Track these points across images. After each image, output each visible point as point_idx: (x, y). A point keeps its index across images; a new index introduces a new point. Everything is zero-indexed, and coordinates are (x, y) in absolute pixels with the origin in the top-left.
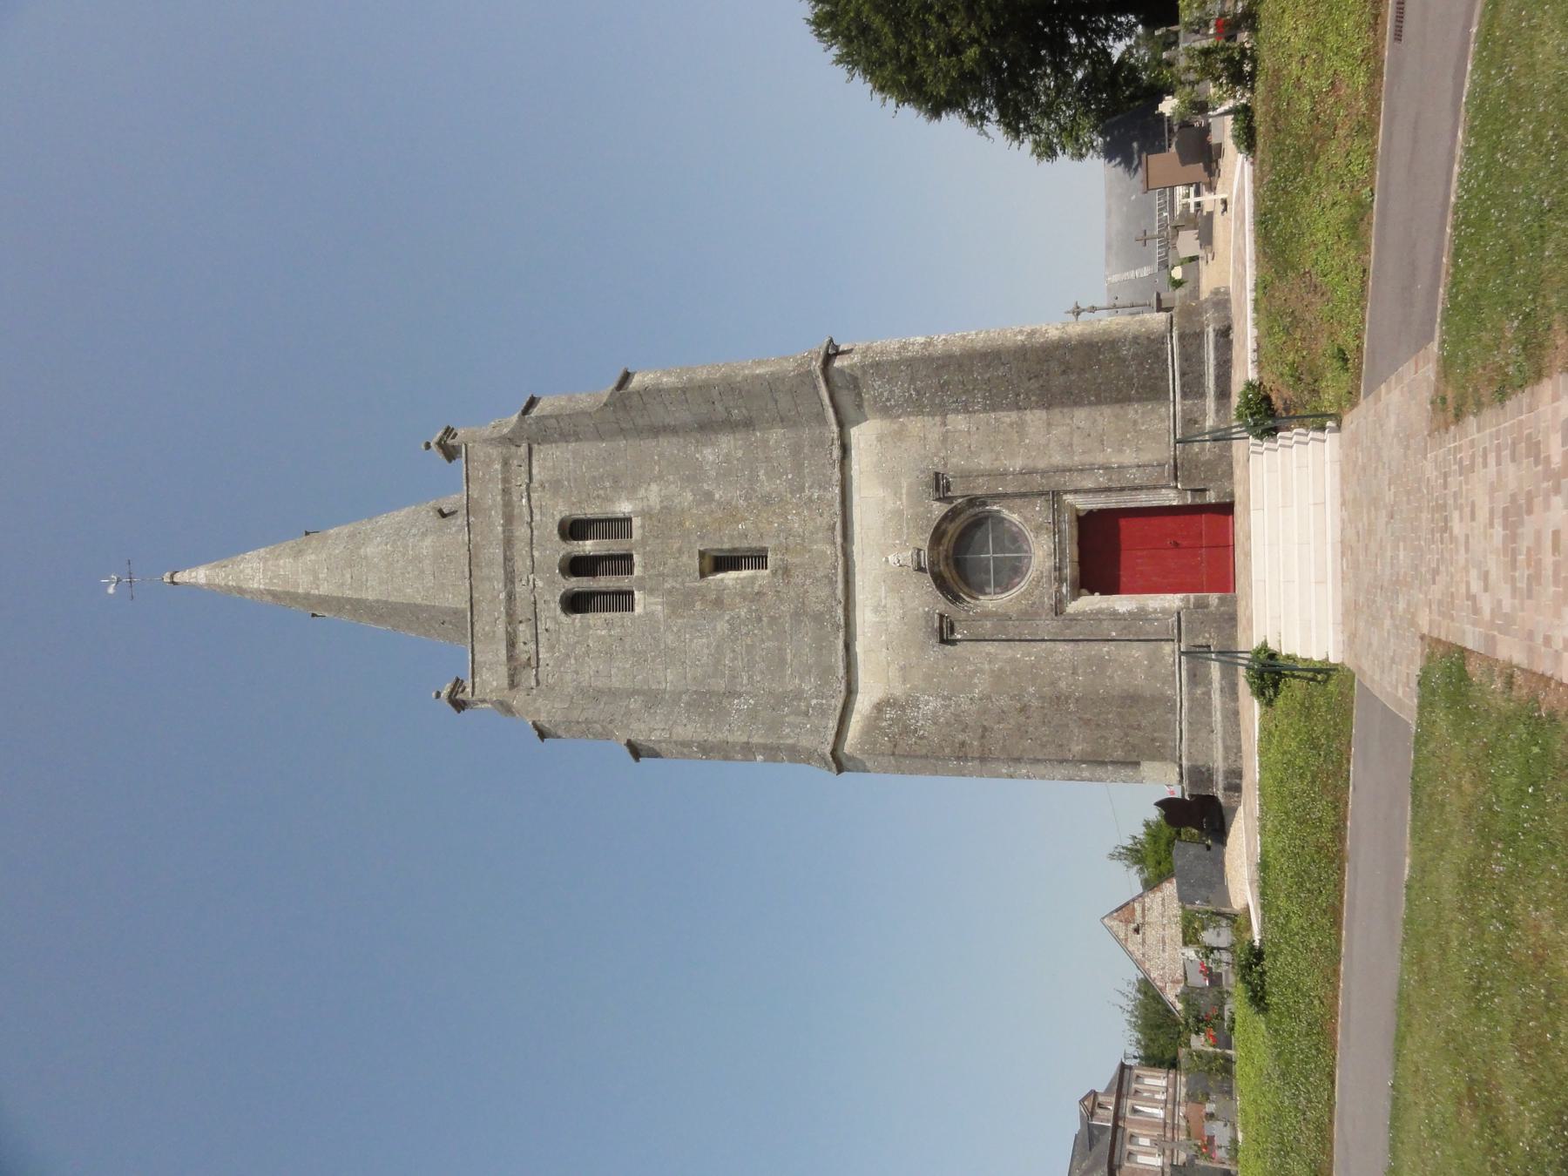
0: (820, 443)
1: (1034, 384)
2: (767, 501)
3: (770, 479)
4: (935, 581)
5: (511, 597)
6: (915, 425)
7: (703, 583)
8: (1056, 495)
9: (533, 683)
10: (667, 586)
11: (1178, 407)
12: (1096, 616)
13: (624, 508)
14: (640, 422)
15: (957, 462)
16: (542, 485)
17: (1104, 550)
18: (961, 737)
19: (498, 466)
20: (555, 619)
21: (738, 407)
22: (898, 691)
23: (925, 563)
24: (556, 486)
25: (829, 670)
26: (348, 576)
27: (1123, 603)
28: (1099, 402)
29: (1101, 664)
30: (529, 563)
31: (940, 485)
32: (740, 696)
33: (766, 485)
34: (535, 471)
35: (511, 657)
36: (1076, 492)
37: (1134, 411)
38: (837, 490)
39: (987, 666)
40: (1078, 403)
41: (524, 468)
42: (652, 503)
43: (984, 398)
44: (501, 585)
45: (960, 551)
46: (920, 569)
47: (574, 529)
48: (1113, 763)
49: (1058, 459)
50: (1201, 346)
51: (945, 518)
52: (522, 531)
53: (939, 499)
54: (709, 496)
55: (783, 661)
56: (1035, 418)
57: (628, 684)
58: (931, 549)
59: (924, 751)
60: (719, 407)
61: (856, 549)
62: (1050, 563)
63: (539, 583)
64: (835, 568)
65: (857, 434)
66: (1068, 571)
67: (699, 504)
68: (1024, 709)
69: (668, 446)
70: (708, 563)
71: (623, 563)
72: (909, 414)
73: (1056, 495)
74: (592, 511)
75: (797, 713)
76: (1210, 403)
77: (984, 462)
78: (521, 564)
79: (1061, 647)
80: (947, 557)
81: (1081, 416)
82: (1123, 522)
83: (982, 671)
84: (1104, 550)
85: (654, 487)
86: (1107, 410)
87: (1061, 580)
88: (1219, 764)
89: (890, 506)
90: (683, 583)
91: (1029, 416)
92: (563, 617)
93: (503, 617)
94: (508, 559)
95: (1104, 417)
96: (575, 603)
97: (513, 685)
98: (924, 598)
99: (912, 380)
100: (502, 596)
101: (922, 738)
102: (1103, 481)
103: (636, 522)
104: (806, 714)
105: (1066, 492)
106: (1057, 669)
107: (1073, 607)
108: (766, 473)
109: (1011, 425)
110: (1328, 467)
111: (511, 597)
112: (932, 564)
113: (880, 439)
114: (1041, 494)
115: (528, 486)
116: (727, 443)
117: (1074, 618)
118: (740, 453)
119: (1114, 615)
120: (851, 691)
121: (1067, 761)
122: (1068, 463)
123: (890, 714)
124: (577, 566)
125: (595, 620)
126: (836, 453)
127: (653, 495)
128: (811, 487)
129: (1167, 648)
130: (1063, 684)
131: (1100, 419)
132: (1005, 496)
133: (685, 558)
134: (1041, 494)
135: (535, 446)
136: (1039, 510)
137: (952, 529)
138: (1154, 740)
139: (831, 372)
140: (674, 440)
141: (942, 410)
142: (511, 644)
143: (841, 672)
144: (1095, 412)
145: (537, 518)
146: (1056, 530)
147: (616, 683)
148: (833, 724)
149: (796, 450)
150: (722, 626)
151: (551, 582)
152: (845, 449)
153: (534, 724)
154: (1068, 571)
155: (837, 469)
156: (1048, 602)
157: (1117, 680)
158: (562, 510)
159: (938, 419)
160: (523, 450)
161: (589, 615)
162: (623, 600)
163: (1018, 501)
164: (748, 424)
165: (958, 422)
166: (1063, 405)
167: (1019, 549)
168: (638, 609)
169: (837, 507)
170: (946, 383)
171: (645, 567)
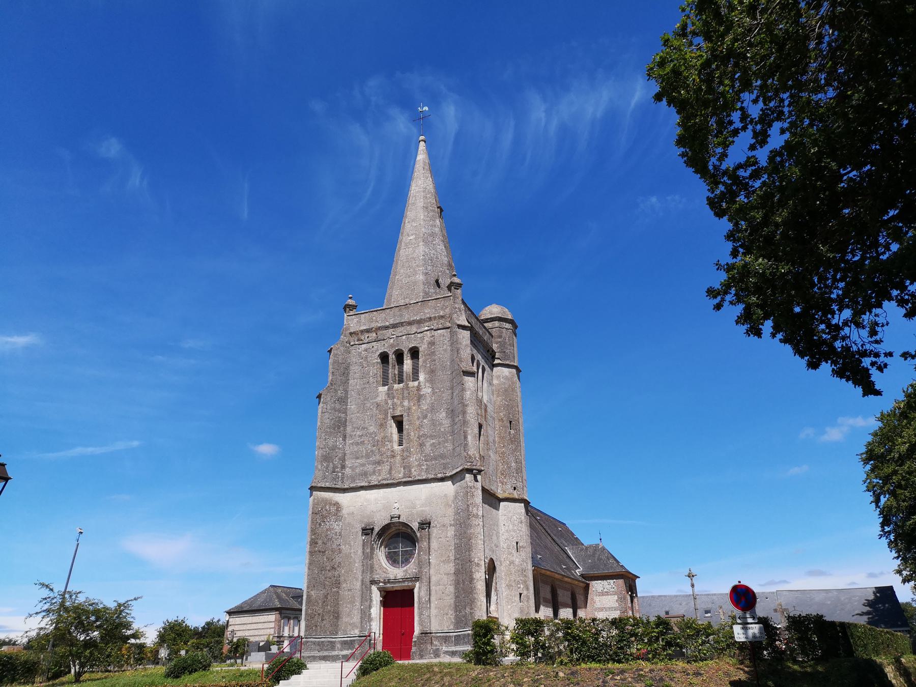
18: (320, 542)
68: (333, 568)
75: (335, 467)
101: (320, 525)
120: (344, 490)
123: (333, 509)
148: (328, 485)
156: (376, 577)
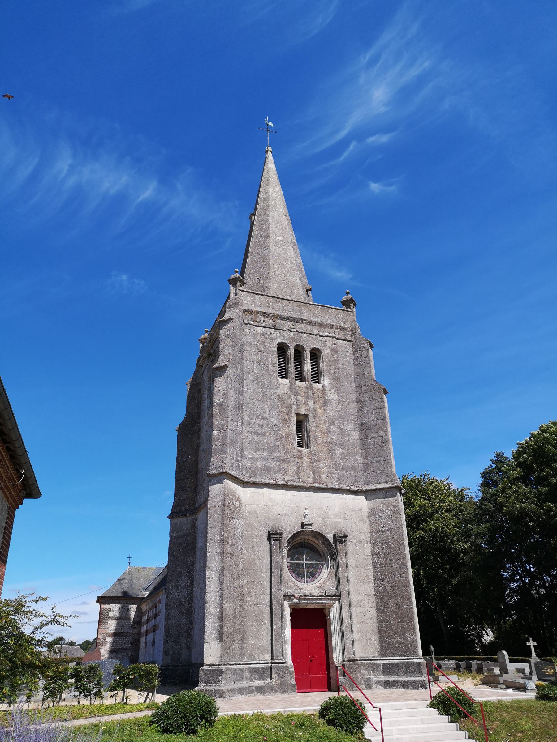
0: (357, 479)
1: (389, 589)
2: (331, 452)
3: (342, 454)
4: (298, 533)
5: (286, 319)
6: (366, 527)
7: (294, 415)
8: (338, 597)
9: (246, 321)
10: (292, 397)
11: (379, 662)
12: (282, 618)
13: (326, 381)
14: (366, 395)
15: (351, 547)
16: (335, 344)
17: (311, 622)
18: (230, 542)
19: (342, 324)
20: (276, 338)
21: (374, 443)
22: (244, 509)
23: (307, 528)
24: (334, 351)
25: (254, 475)
26: (280, 238)
27: (288, 632)
28: (379, 622)
29: (260, 620)
30: (301, 331)
31: (340, 538)
32: (242, 426)
33: (338, 451)
34: (341, 341)
35: (258, 312)
36: (340, 608)
37: (375, 639)
38: (337, 487)
39: (257, 557)
40: (378, 610)
41: (343, 337)
42: (329, 395)
43: (380, 564)
44: (291, 315)
45: (310, 548)
46: (303, 525)
47: (315, 355)
48: (221, 627)
49: (354, 599)
50: (413, 673)
51: (326, 540)
52: (315, 330)
53: (334, 535)
54: (332, 423)
55: (258, 450)
56: (370, 588)
57: (245, 369)
58: (312, 531)
59: (225, 522)
60: (374, 435)
61: (311, 493)
62: (307, 593)
63: (292, 334)
64: (302, 482)
65: (361, 498)
66: (303, 603)
67: (329, 418)
69: (353, 407)
70: (301, 418)
71: (301, 377)
72: (371, 525)
73: (338, 597)
74: (324, 364)
76: (383, 678)
77: (352, 562)
78: (299, 326)
79: (268, 598)
80: (305, 539)
81: (373, 612)
82: (321, 631)
83: (254, 555)
84: (311, 622)
85: (335, 397)
86: (375, 625)
87: (299, 599)
88: (224, 686)
89: (331, 512)
90: (293, 404)
91: (372, 585)
92: (277, 342)
93: (277, 313)
94: (302, 321)
95: (372, 624)
96: (282, 349)
97: (245, 311)
98: (290, 528)
99: (390, 529)
100: (286, 315)
102: (345, 622)
103: (320, 386)
104: (237, 460)
105: (340, 603)
106: (256, 595)
107: (286, 604)
108: (343, 453)
109: (367, 576)
110: (511, 697)
111: (286, 319)
112: (305, 531)
113: (360, 510)
114: (339, 590)
115: (335, 337)
116: (355, 436)
117: (282, 606)
118: (351, 441)
119: (282, 628)
120: (244, 484)
121: (222, 600)
122: (352, 604)
124: (299, 352)
125: (274, 358)
126: (354, 488)
127: (332, 396)
128: (338, 474)
129: (268, 657)
130: (249, 598)
131: (371, 621)
132: (337, 571)
133: (304, 407)
134: (339, 590)
135: (351, 344)
136: (331, 588)
137: (318, 543)
138: (229, 649)
139: (395, 491)
140: (356, 410)
141: (374, 542)
142: (265, 315)
143: (254, 480)
144: (375, 619)
145: (321, 338)
146: (323, 598)
147: (246, 363)
149: (353, 468)
150: (274, 421)
151: (292, 339)
152: (355, 493)
153: (232, 319)
154: (303, 603)
155: (346, 488)
156: (290, 592)
157: (251, 629)
158: (326, 352)
159: (369, 540)
160: (350, 338)
161: (276, 355)
162: (284, 373)
163: (334, 578)
164: (364, 446)
165: (368, 550)
166: (377, 603)
167: (308, 577)
168: (281, 380)
169: (329, 486)
170: (389, 546)
171: (300, 387)
